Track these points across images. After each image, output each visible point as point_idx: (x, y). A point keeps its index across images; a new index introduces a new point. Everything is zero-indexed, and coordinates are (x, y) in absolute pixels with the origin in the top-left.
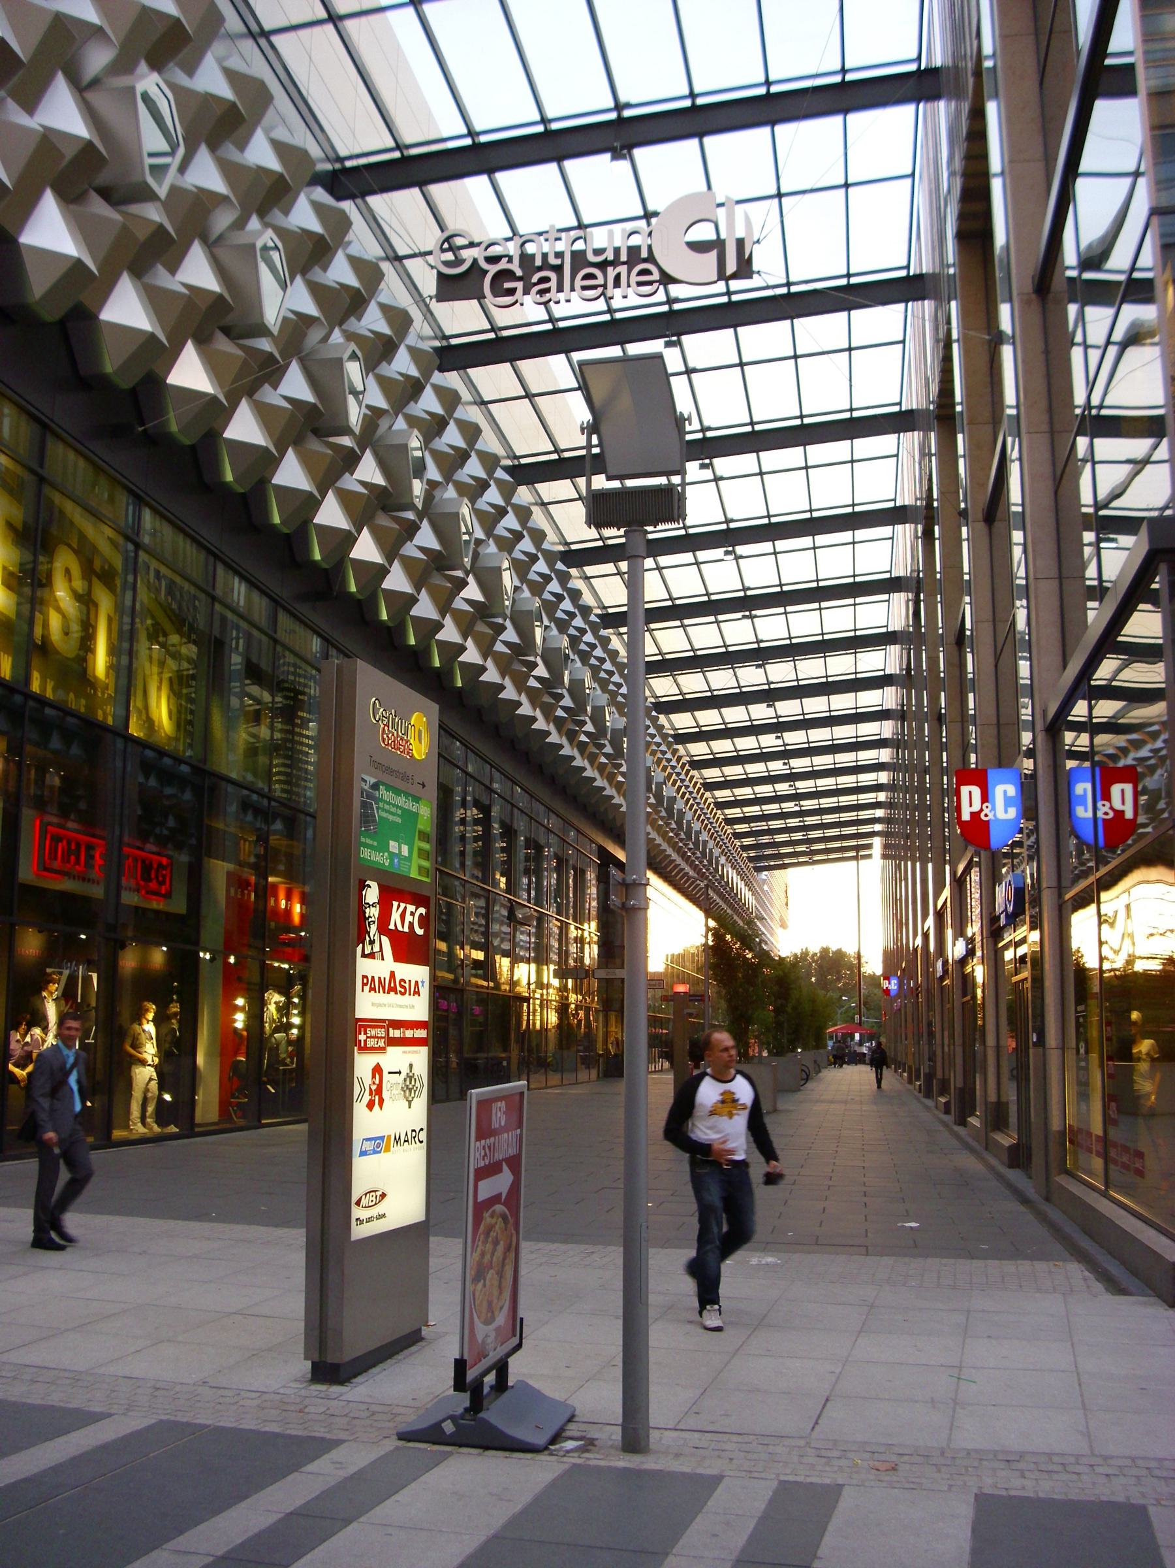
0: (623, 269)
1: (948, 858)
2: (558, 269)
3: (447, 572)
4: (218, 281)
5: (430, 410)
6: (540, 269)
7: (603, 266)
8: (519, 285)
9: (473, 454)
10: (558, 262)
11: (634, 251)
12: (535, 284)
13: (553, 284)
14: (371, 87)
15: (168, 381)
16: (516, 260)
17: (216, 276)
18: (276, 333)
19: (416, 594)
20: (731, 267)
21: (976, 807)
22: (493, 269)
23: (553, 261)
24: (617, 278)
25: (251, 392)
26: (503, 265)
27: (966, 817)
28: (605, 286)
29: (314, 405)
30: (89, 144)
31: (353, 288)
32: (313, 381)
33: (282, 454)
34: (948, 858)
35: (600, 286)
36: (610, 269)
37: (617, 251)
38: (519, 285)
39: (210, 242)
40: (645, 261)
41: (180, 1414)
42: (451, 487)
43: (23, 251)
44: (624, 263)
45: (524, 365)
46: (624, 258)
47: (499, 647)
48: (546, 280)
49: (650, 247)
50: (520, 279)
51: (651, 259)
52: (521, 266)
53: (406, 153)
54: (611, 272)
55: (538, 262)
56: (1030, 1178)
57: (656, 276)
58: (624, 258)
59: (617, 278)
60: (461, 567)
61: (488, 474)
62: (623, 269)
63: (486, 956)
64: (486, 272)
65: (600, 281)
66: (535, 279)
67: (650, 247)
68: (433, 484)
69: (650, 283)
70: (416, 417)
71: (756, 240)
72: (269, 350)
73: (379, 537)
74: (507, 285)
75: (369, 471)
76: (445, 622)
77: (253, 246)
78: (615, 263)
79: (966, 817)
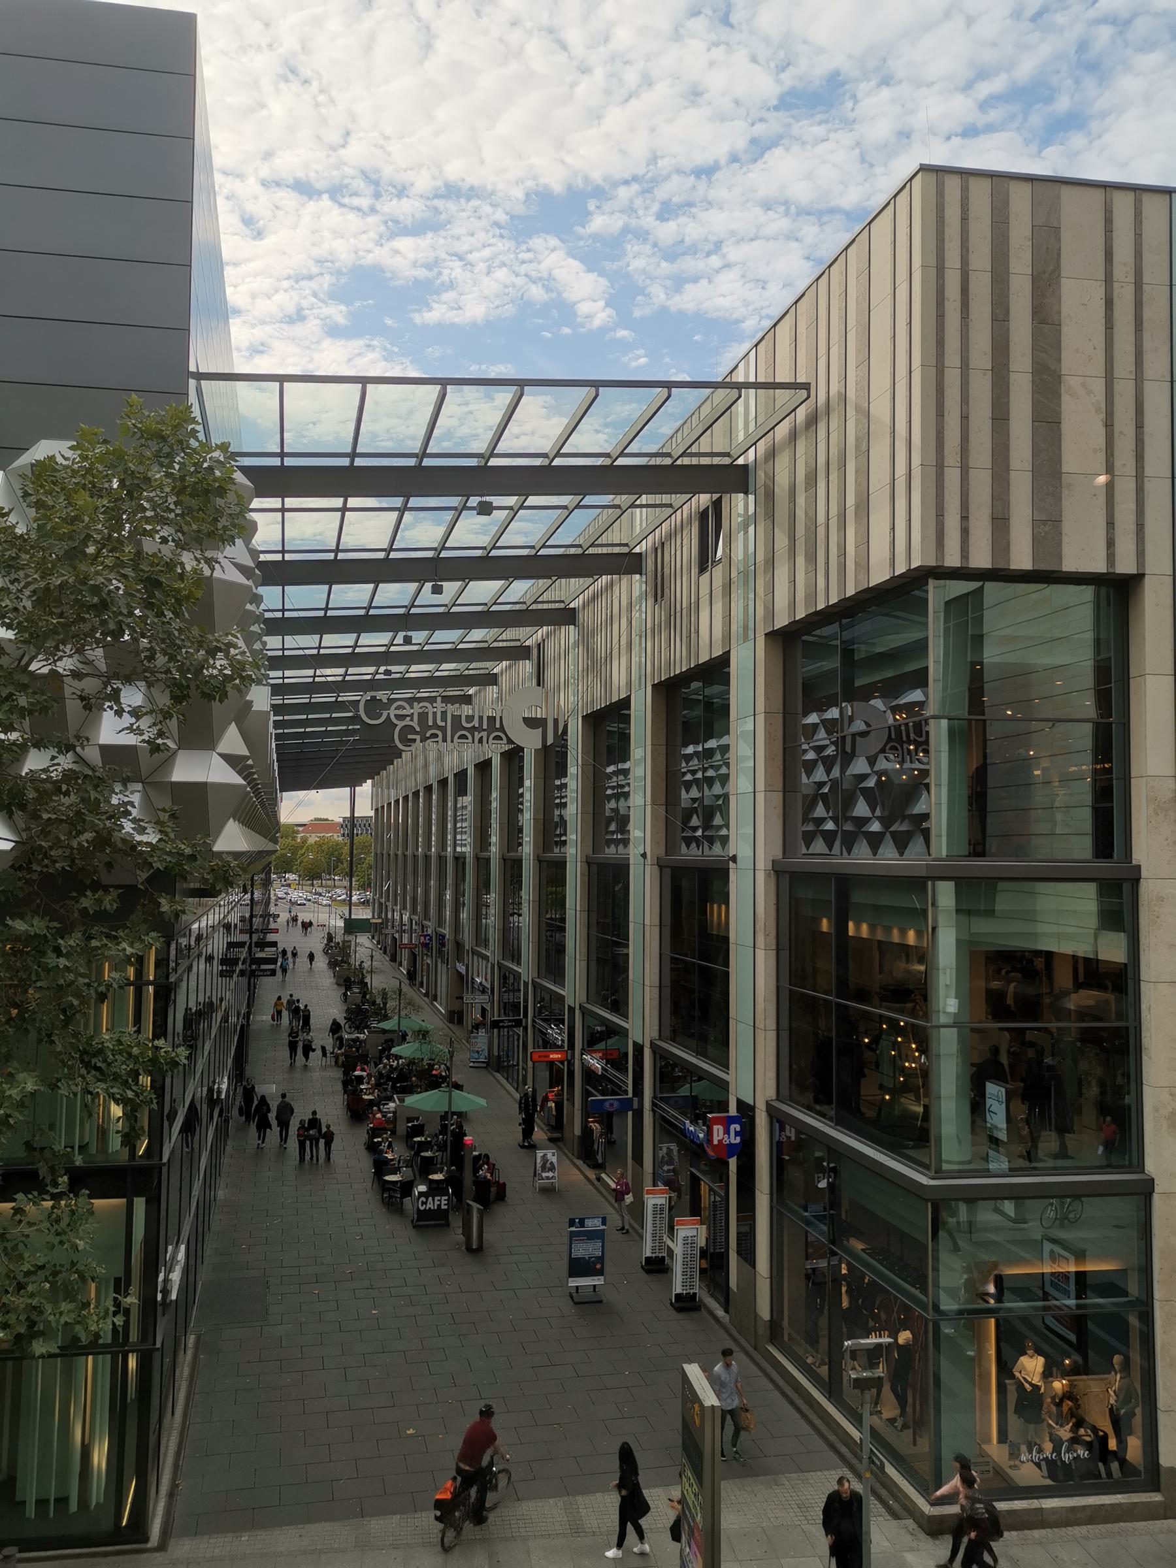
1: (132, 1362)
6: (430, 728)
8: (418, 737)
13: (440, 739)
21: (720, 1138)
22: (400, 724)
26: (407, 722)
27: (715, 1142)
34: (132, 1362)
38: (418, 737)
41: (910, 1529)
44: (484, 730)
48: (436, 736)
50: (417, 733)
51: (502, 729)
62: (484, 734)
63: (105, 1345)
79: (715, 1142)
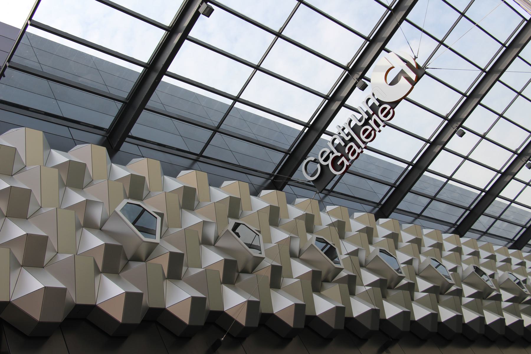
0: (374, 117)
2: (352, 140)
3: (523, 302)
4: (431, 283)
5: (430, 245)
6: (345, 146)
7: (366, 123)
9: (480, 250)
10: (350, 137)
11: (373, 107)
12: (348, 153)
13: (355, 147)
14: (370, 178)
15: (354, 317)
16: (335, 151)
17: (470, 287)
18: (530, 294)
19: (520, 319)
20: (413, 76)
22: (329, 162)
23: (347, 138)
24: (375, 122)
25: (352, 293)
26: (332, 157)
28: (373, 129)
29: (380, 279)
30: (313, 271)
31: (414, 239)
32: (373, 271)
33: (437, 310)
35: (371, 131)
36: (370, 121)
37: (367, 113)
39: (298, 254)
40: (380, 106)
42: (499, 271)
43: (319, 317)
44: (373, 114)
45: (488, 211)
46: (371, 112)
47: (505, 305)
49: (378, 100)
51: (381, 103)
52: (338, 152)
53: (396, 186)
54: (371, 122)
55: (343, 144)
56: (318, 168)
57: (388, 107)
58: (371, 112)
59: (375, 122)
60: (493, 290)
61: (520, 259)
62: (374, 117)
64: (328, 165)
65: (370, 129)
66: (347, 151)
67: (378, 100)
68: (492, 276)
69: (388, 113)
70: (501, 266)
71: (414, 58)
72: (456, 288)
73: (491, 310)
74: (339, 163)
75: (423, 285)
76: (523, 319)
77: (312, 245)
78: (370, 118)
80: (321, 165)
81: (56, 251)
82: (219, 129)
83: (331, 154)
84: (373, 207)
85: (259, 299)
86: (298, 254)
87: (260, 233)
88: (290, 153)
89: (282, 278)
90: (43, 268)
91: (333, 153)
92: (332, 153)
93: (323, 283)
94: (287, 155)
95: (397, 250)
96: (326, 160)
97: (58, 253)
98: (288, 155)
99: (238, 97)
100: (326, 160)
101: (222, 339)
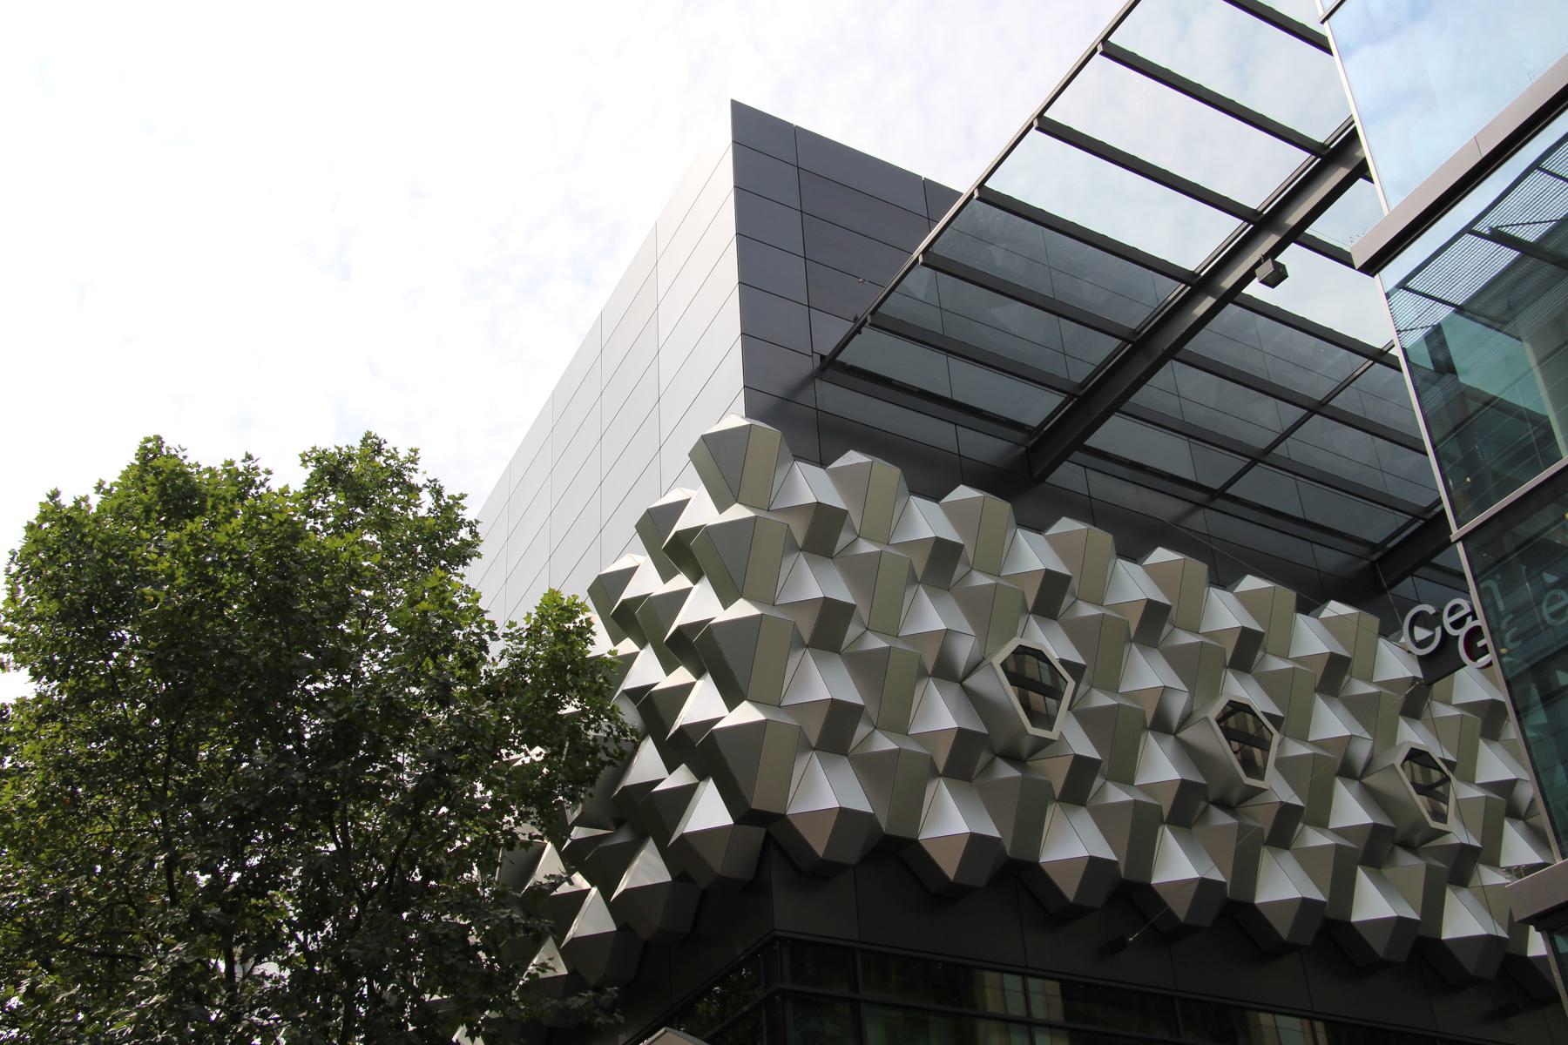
12: (1507, 631)
22: (1461, 633)
26: (1470, 624)
64: (1458, 637)
80: (1444, 631)
81: (856, 533)
82: (1271, 454)
83: (1469, 618)
84: (1008, 444)
85: (1349, 652)
86: (1359, 772)
87: (1278, 728)
88: (1429, 516)
89: (1347, 677)
90: (832, 558)
91: (1475, 618)
92: (1473, 614)
93: (1396, 847)
94: (1416, 521)
95: (1508, 821)
96: (1458, 624)
97: (859, 536)
98: (1422, 522)
99: (1324, 402)
100: (1458, 624)
101: (1131, 939)
